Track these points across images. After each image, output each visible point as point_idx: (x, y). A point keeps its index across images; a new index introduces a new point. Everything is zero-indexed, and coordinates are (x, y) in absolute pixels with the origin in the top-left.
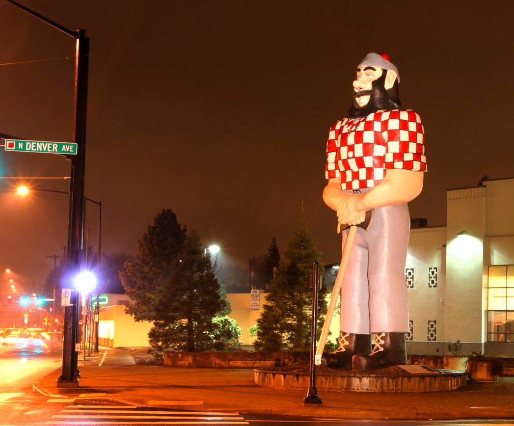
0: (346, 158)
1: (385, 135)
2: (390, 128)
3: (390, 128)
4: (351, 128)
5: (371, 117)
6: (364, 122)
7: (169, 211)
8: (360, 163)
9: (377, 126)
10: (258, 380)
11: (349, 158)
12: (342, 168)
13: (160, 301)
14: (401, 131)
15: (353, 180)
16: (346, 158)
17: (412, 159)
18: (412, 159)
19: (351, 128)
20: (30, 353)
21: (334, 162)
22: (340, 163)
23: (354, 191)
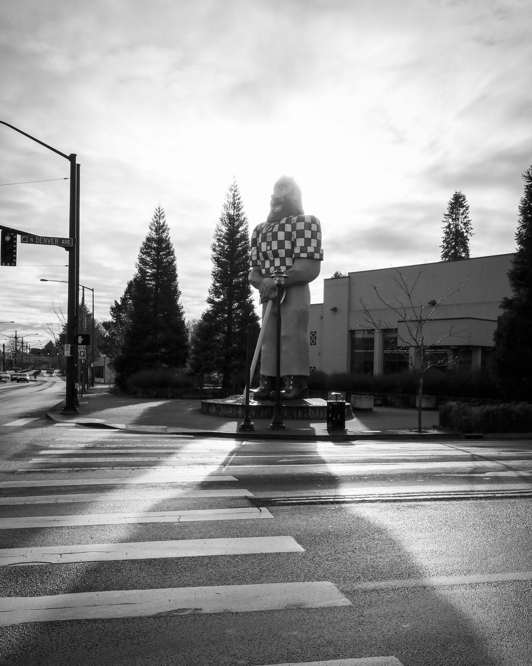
1: (294, 233)
4: (269, 229)
8: (276, 254)
9: (288, 228)
12: (262, 259)
17: (313, 251)
18: (313, 251)
22: (261, 254)
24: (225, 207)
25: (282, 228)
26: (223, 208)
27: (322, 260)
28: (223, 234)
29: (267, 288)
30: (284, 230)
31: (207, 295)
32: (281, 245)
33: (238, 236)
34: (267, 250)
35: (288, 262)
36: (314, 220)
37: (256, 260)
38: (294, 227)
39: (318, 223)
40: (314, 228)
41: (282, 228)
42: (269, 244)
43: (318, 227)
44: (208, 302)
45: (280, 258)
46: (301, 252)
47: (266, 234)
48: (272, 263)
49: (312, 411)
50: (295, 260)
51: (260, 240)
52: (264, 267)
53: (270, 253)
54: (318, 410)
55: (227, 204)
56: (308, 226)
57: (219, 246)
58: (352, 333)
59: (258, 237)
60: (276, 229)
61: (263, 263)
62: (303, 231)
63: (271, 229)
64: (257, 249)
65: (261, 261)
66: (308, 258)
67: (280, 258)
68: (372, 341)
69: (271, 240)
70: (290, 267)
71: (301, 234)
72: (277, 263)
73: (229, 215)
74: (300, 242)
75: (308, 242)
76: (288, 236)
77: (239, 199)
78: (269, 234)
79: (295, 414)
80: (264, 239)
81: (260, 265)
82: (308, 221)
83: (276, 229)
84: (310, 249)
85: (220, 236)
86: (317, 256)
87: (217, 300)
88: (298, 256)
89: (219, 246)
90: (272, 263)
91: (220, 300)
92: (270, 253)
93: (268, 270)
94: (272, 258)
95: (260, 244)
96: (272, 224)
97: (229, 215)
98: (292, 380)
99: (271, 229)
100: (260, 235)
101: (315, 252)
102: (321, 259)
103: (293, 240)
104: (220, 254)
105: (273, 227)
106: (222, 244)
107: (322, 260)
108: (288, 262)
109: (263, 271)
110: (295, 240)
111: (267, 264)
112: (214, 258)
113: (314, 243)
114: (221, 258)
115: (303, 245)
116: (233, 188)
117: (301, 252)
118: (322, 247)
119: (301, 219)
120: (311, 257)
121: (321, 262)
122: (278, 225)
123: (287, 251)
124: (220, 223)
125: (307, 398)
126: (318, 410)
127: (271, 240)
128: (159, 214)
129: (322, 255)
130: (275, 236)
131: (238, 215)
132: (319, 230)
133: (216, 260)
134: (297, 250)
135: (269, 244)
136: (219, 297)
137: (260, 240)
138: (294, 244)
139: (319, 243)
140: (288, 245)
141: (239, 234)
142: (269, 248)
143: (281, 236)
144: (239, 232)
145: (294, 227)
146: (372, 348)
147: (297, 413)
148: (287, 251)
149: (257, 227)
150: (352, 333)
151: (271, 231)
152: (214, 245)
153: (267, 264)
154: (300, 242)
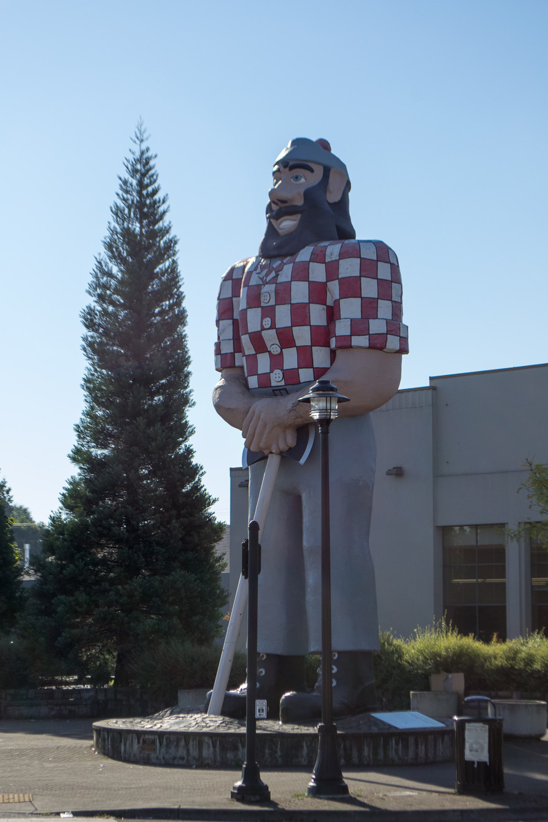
0: (259, 329)
1: (334, 287)
2: (343, 273)
3: (343, 273)
4: (267, 275)
5: (304, 255)
6: (291, 265)
7: (300, 144)
8: (286, 339)
9: (318, 272)
10: (95, 726)
11: (263, 329)
12: (248, 348)
13: (194, 516)
14: (311, 305)
15: (272, 371)
16: (259, 329)
17: (384, 330)
18: (384, 330)
19: (267, 275)
20: (426, 754)
21: (231, 338)
22: (245, 339)
23: (273, 391)
24: (117, 212)
25: (301, 273)
26: (110, 217)
27: (406, 351)
28: (113, 282)
29: (265, 425)
30: (305, 278)
31: (72, 441)
32: (300, 315)
33: (154, 285)
34: (263, 329)
35: (320, 357)
36: (383, 252)
37: (233, 355)
38: (332, 271)
39: (392, 260)
40: (384, 271)
41: (301, 273)
42: (269, 312)
43: (395, 269)
44: (74, 460)
45: (298, 348)
46: (354, 333)
47: (259, 287)
48: (277, 361)
49: (397, 743)
50: (338, 352)
51: (242, 302)
52: (253, 371)
53: (270, 338)
54: (411, 740)
55: (121, 204)
56: (368, 268)
57: (105, 313)
58: (444, 531)
59: (236, 293)
60: (286, 275)
61: (252, 360)
62: (358, 279)
63: (273, 274)
64: (235, 323)
65: (248, 357)
66: (371, 347)
67: (298, 348)
68: (499, 553)
69: (272, 302)
70: (324, 371)
71: (351, 288)
72: (291, 359)
73: (127, 233)
74: (351, 309)
75: (369, 308)
76: (318, 293)
77: (155, 192)
78: (269, 289)
79: (355, 753)
80: (254, 300)
81: (242, 367)
82: (370, 254)
83: (286, 275)
84: (377, 326)
85: (105, 287)
86: (393, 343)
87: (98, 452)
88: (345, 343)
89: (105, 313)
90: (277, 361)
91: (106, 452)
92: (270, 338)
93: (264, 380)
94: (276, 350)
95: (244, 313)
96: (277, 263)
97: (127, 233)
98: (336, 663)
99: (273, 274)
100: (243, 291)
101: (389, 332)
102: (404, 350)
103: (330, 302)
104: (106, 333)
105: (278, 270)
106: (111, 308)
107: (406, 351)
108: (320, 357)
109: (253, 382)
110: (337, 302)
111: (264, 363)
112: (91, 345)
113: (384, 309)
114: (107, 344)
115: (357, 314)
116: (139, 167)
117: (354, 333)
118: (406, 320)
119: (355, 251)
120: (377, 345)
121: (404, 356)
122: (291, 265)
123: (315, 330)
124: (104, 254)
125: (375, 710)
126: (411, 740)
127: (272, 302)
128: (142, 170)
129: (404, 340)
130: (283, 294)
131: (154, 235)
132: (396, 277)
133: (94, 351)
134: (342, 328)
135: (269, 312)
136: (104, 446)
137: (242, 302)
138: (333, 314)
139: (397, 310)
140: (317, 315)
141: (156, 281)
142: (267, 322)
143: (300, 292)
144: (153, 276)
145: (332, 271)
146: (501, 573)
147: (360, 751)
148: (315, 330)
149: (233, 269)
150: (444, 531)
151: (274, 280)
152: (91, 311)
153: (264, 363)
154: (351, 309)
